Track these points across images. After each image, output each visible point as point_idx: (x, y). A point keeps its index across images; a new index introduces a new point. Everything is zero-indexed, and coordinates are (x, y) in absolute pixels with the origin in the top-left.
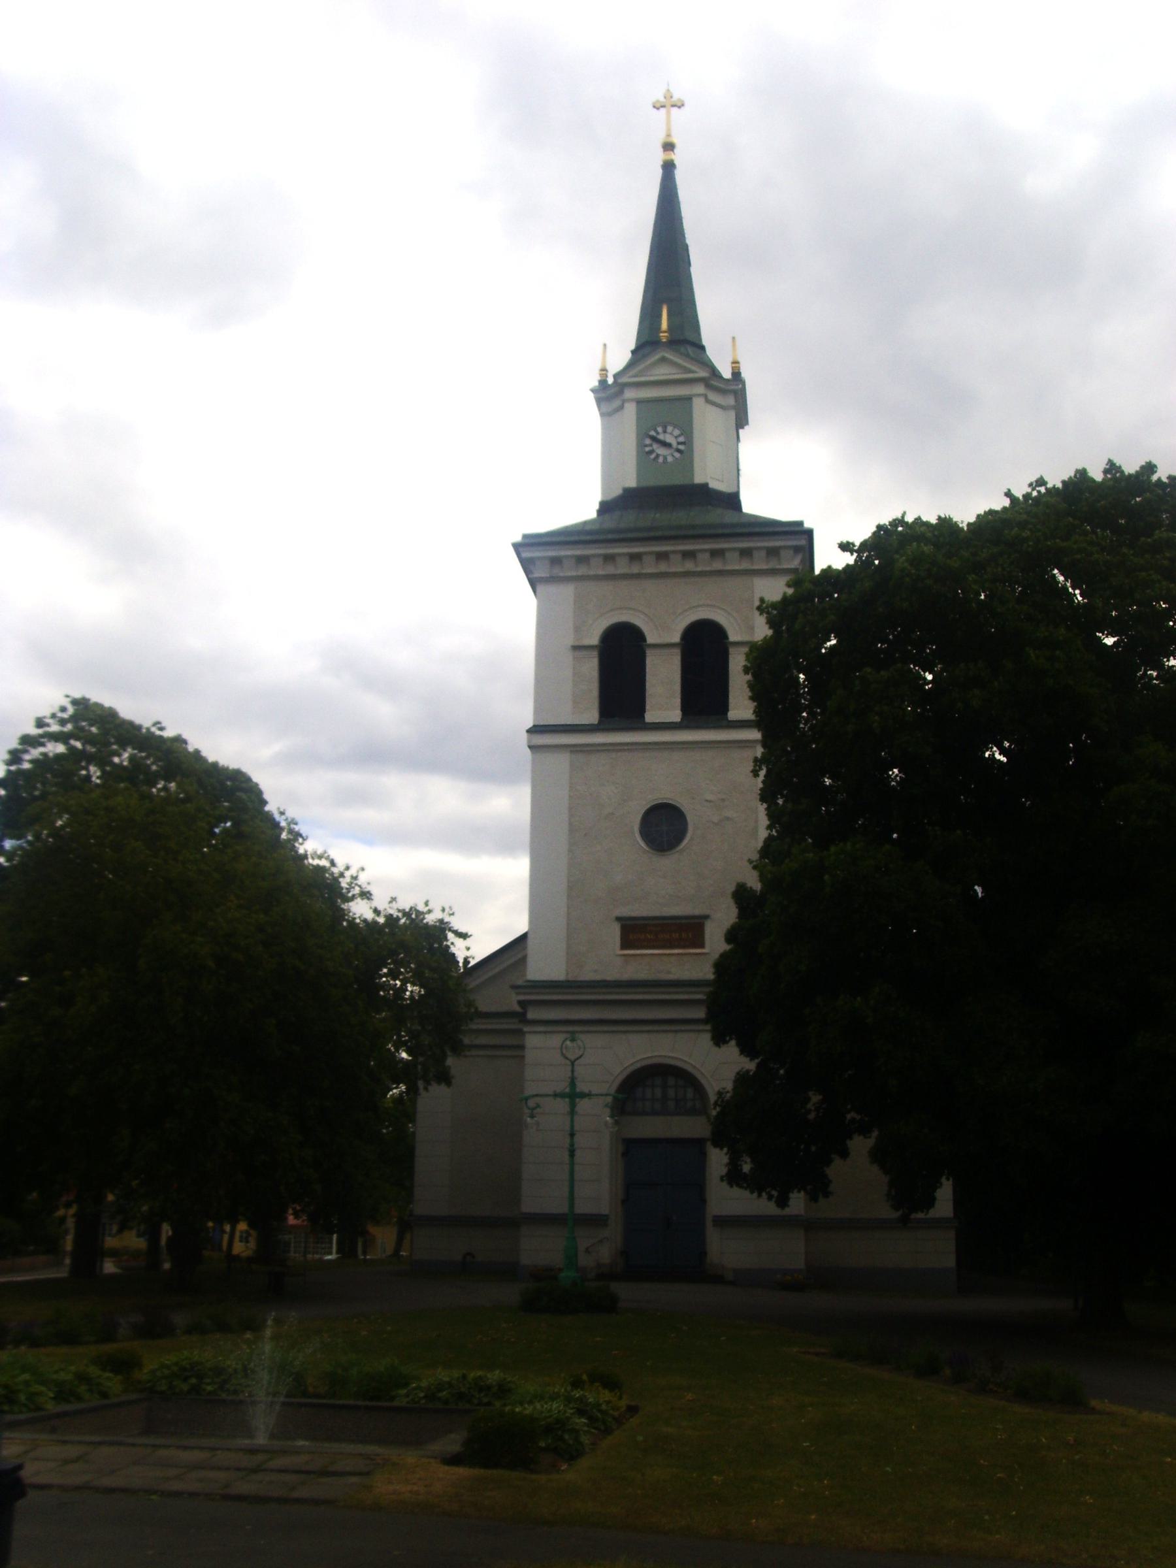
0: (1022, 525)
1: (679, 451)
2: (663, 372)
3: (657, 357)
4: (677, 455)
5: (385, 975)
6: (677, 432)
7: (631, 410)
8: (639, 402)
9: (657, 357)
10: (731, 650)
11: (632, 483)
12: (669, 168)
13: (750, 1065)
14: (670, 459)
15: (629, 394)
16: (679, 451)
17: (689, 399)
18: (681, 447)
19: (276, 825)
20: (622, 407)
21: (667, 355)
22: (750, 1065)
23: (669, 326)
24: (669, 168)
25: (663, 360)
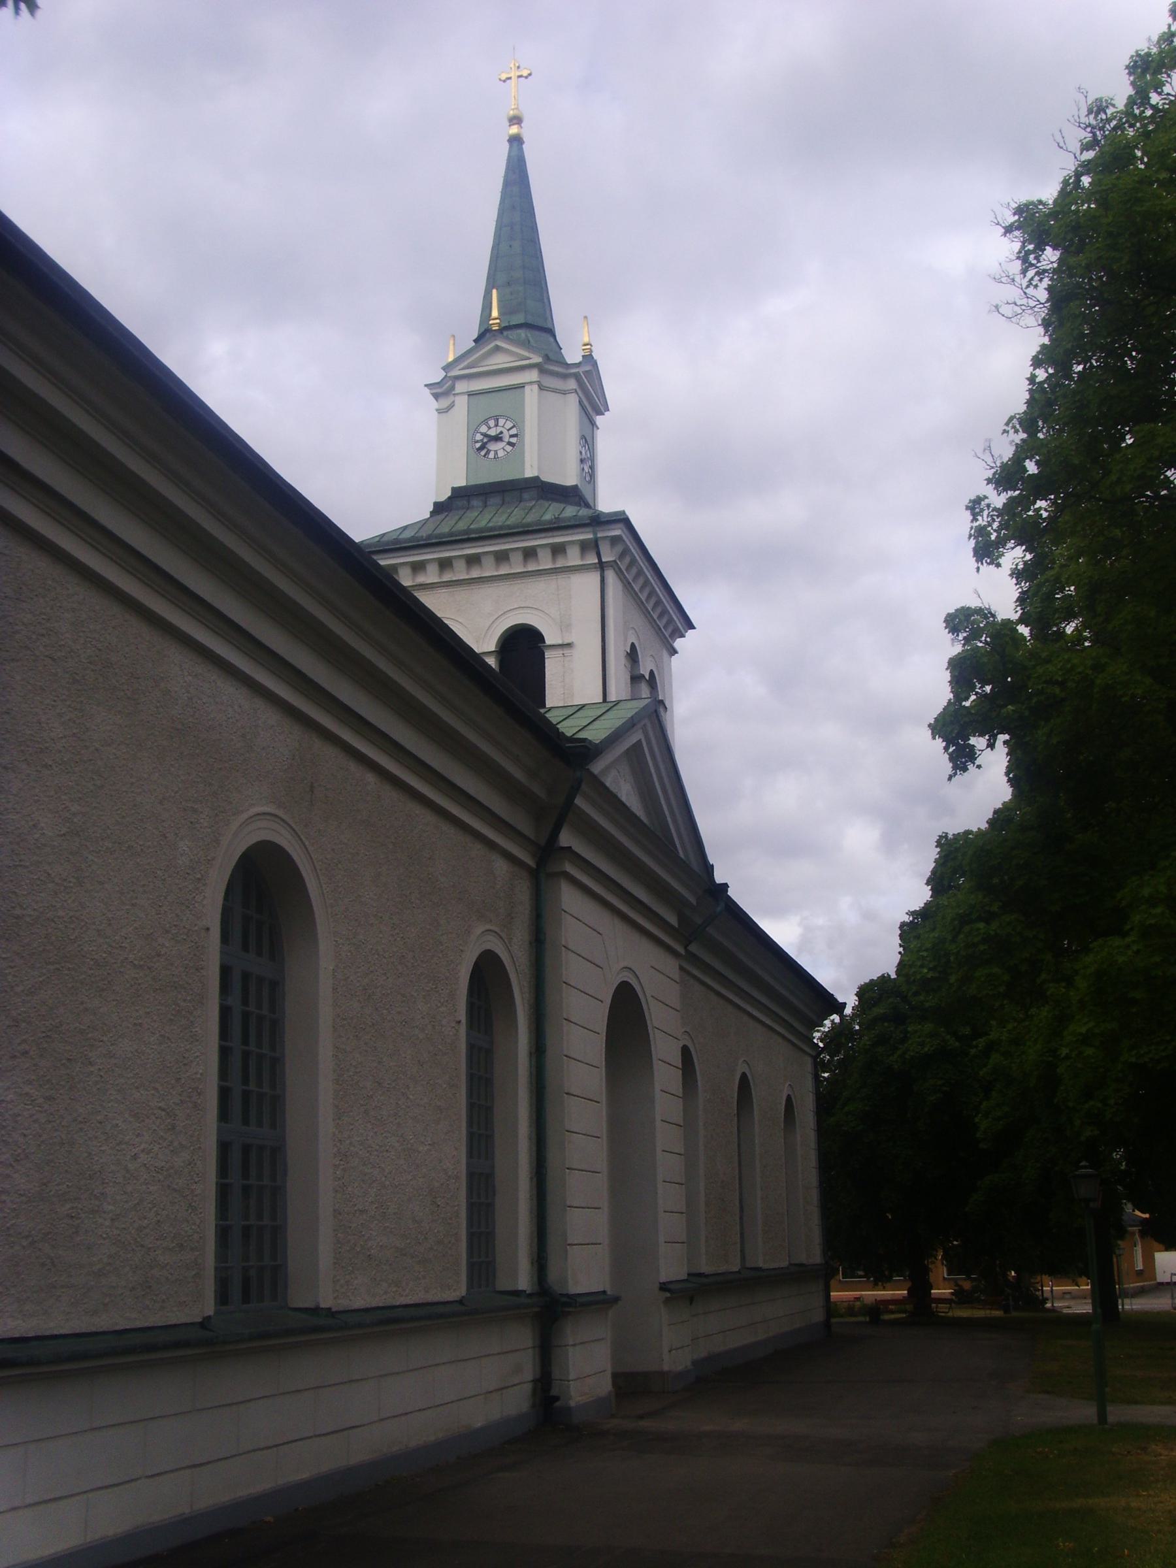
0: (1079, 351)
1: (509, 443)
2: (500, 361)
3: (492, 345)
4: (509, 448)
5: (1086, 639)
6: (509, 425)
7: (462, 403)
8: (471, 394)
9: (492, 345)
10: (548, 654)
11: (462, 482)
12: (516, 141)
13: (893, 976)
14: (501, 454)
15: (461, 387)
16: (509, 443)
17: (521, 386)
18: (513, 440)
19: (1060, 301)
20: (452, 406)
21: (499, 343)
22: (893, 976)
23: (500, 313)
24: (516, 141)
25: (498, 349)
